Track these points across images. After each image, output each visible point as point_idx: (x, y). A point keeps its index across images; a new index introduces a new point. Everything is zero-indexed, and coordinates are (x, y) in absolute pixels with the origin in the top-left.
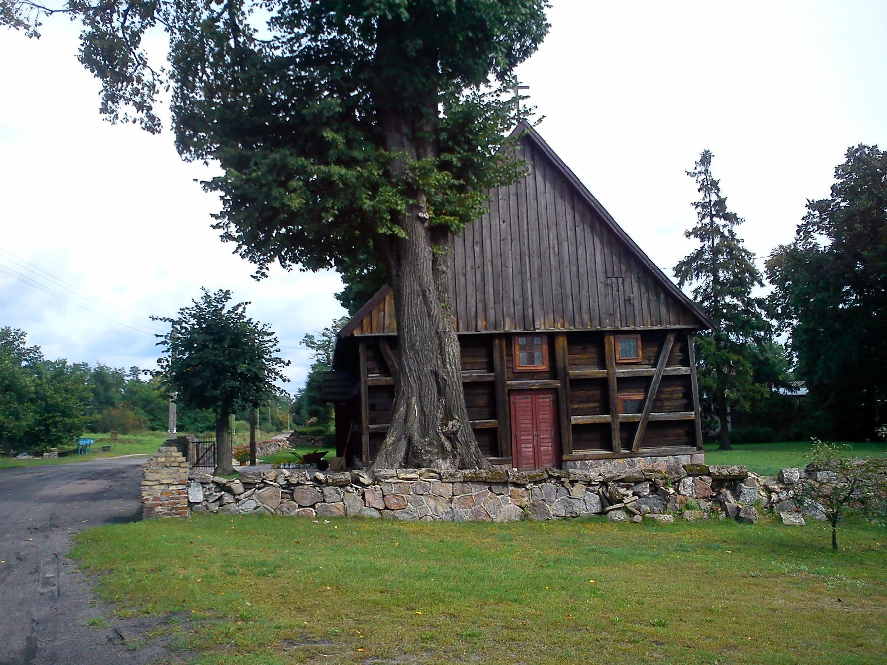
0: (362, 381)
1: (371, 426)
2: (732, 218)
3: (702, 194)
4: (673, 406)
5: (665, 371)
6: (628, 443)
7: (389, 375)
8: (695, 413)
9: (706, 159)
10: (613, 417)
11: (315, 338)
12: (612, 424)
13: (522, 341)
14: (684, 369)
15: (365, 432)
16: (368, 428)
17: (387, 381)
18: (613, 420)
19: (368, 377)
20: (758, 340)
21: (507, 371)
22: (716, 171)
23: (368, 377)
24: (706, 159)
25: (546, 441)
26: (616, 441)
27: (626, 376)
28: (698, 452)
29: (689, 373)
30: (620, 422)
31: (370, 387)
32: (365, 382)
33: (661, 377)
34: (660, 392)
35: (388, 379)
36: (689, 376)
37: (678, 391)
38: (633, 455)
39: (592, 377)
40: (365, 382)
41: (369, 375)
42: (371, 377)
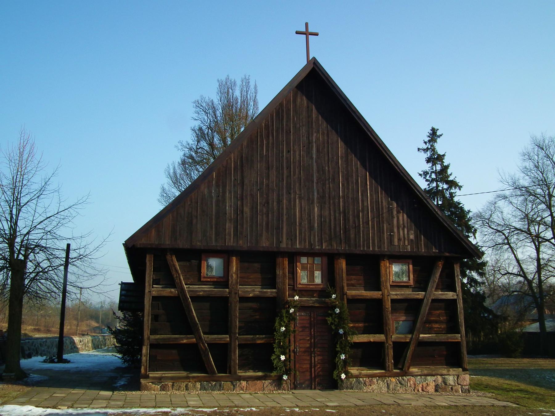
0: (147, 290)
1: (152, 337)
2: (453, 184)
3: (430, 165)
4: (441, 328)
5: (434, 294)
6: (399, 361)
7: (174, 286)
8: (461, 336)
9: (434, 135)
10: (386, 336)
11: (193, 126)
12: (386, 343)
13: (304, 260)
14: (451, 294)
15: (146, 342)
16: (149, 338)
17: (171, 292)
18: (387, 339)
19: (153, 287)
20: (277, 339)
21: (288, 288)
22: (440, 147)
23: (153, 287)
24: (434, 135)
25: (306, 362)
26: (390, 361)
27: (399, 297)
28: (463, 373)
29: (455, 297)
30: (394, 343)
31: (154, 298)
32: (150, 292)
33: (430, 301)
34: (430, 313)
35: (173, 290)
36: (455, 300)
37: (441, 315)
38: (405, 373)
39: (368, 298)
40: (150, 292)
41: (154, 286)
42: (156, 288)
